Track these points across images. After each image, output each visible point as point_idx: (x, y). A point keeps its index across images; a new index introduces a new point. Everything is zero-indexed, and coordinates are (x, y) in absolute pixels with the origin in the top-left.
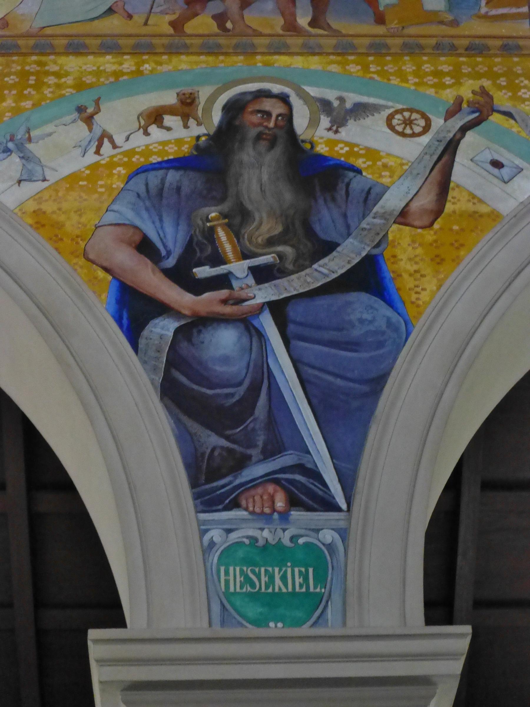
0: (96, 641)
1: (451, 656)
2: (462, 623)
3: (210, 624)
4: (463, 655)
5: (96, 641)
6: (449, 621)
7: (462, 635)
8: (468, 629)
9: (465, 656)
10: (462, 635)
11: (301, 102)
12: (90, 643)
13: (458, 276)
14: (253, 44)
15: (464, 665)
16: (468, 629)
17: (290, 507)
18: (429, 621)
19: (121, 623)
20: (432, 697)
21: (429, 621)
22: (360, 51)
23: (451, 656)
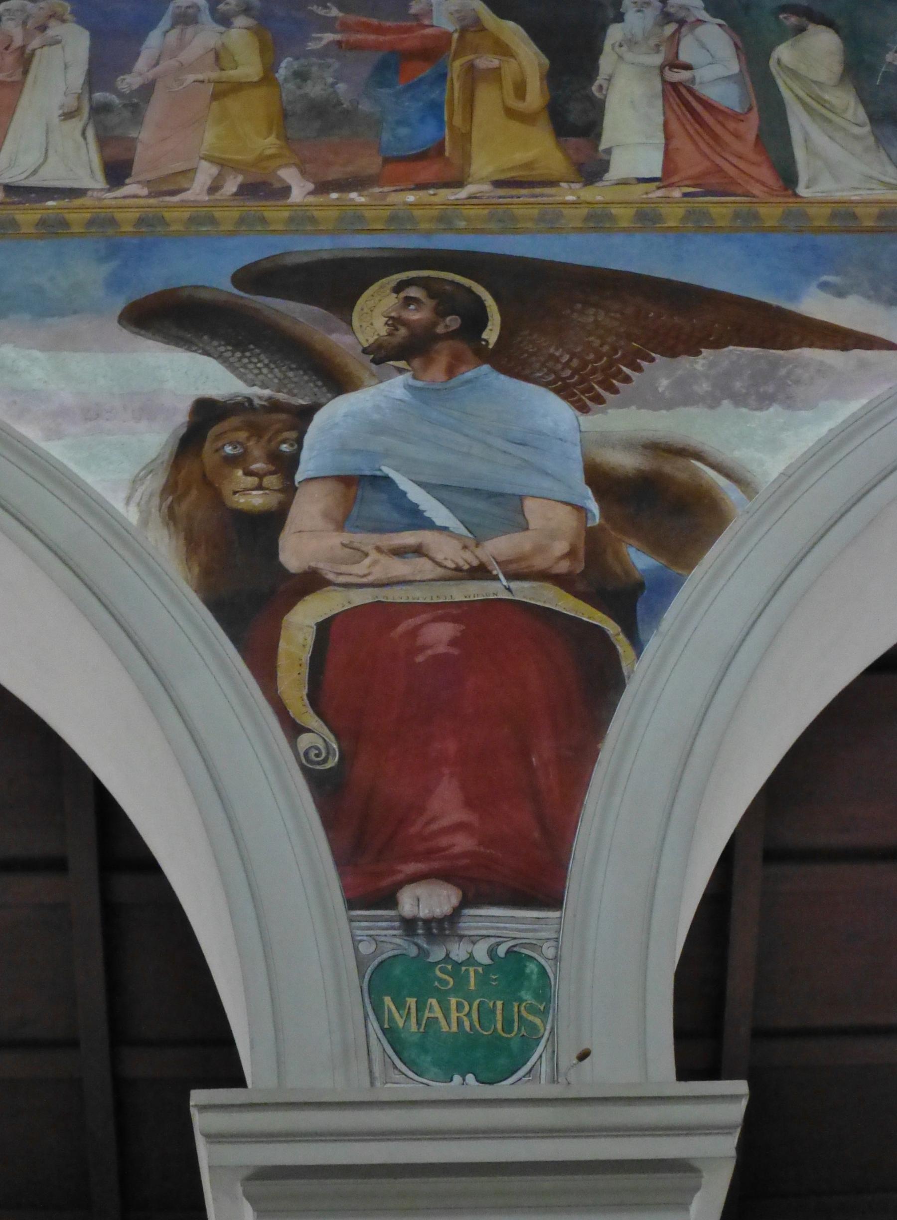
0: (203, 1108)
1: (720, 1129)
2: (731, 1077)
3: (372, 1084)
4: (737, 1127)
5: (203, 1108)
6: (713, 1073)
7: (734, 1098)
8: (741, 1087)
9: (739, 1130)
10: (734, 1098)
11: (464, 534)
12: (194, 1112)
13: (691, 593)
14: (264, 218)
15: (739, 1139)
16: (741, 1087)
17: (480, 561)
18: (685, 1073)
19: (239, 1081)
20: (697, 1189)
21: (685, 1073)
22: (817, 223)
23: (720, 1129)
